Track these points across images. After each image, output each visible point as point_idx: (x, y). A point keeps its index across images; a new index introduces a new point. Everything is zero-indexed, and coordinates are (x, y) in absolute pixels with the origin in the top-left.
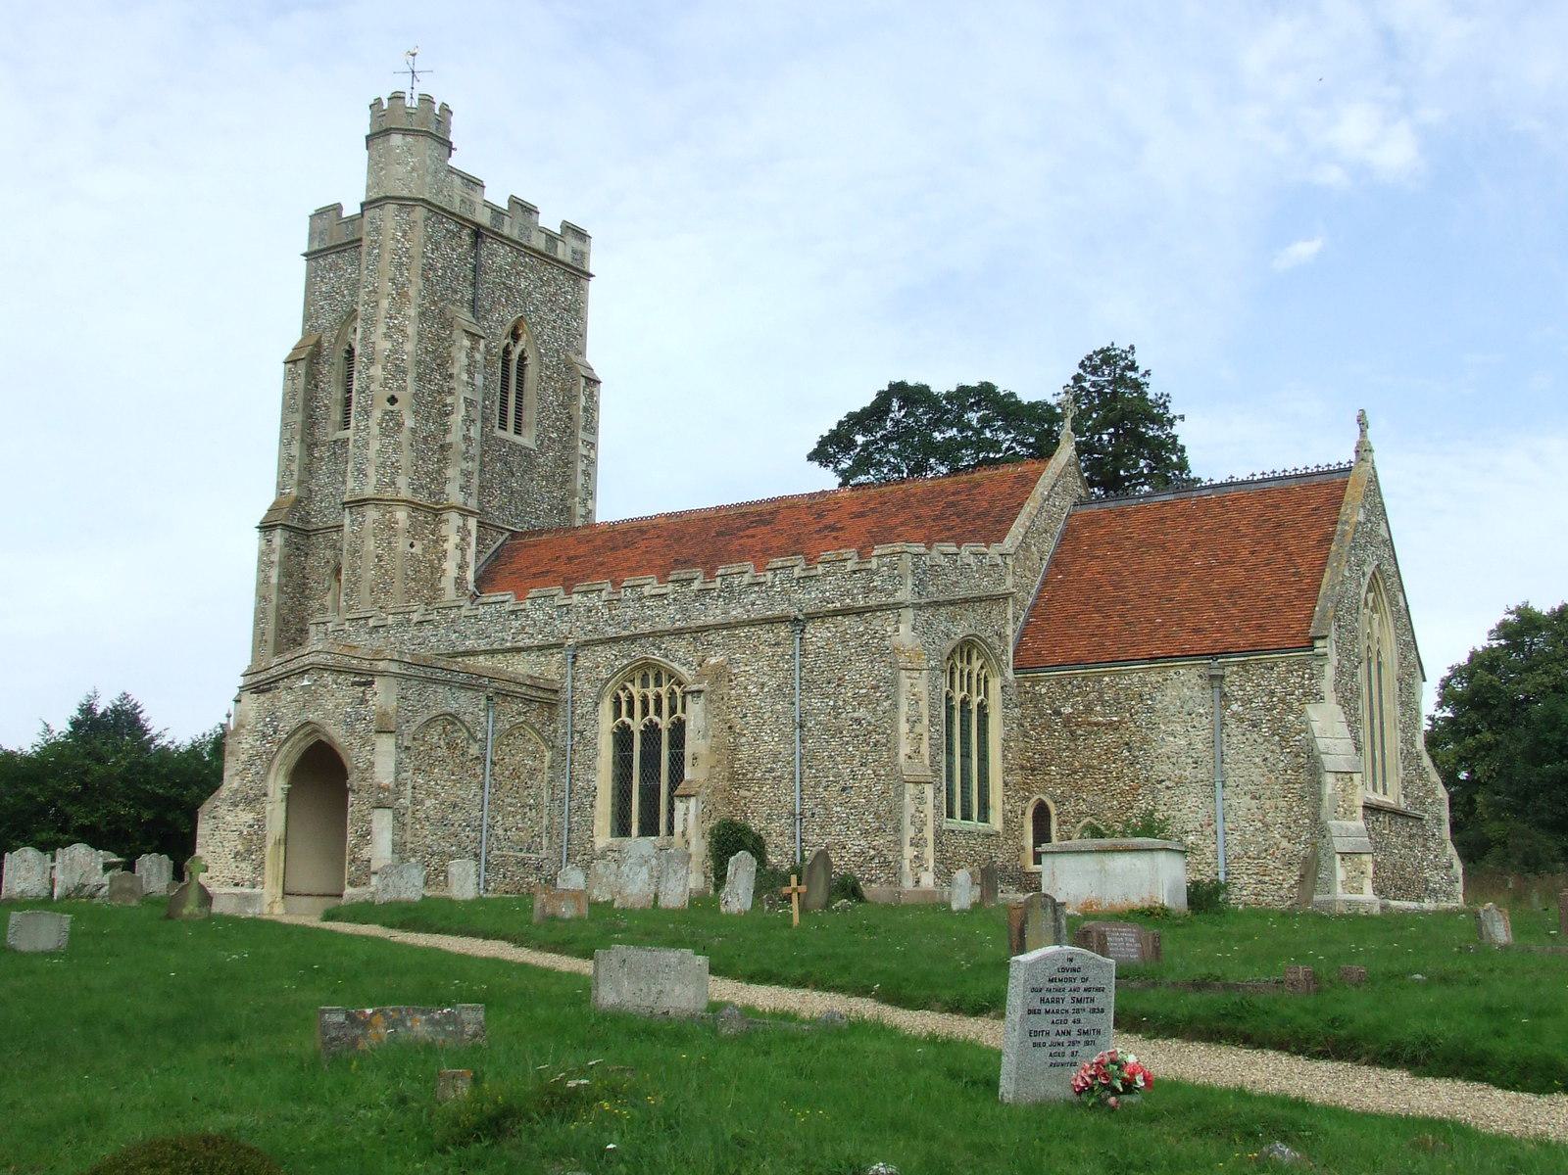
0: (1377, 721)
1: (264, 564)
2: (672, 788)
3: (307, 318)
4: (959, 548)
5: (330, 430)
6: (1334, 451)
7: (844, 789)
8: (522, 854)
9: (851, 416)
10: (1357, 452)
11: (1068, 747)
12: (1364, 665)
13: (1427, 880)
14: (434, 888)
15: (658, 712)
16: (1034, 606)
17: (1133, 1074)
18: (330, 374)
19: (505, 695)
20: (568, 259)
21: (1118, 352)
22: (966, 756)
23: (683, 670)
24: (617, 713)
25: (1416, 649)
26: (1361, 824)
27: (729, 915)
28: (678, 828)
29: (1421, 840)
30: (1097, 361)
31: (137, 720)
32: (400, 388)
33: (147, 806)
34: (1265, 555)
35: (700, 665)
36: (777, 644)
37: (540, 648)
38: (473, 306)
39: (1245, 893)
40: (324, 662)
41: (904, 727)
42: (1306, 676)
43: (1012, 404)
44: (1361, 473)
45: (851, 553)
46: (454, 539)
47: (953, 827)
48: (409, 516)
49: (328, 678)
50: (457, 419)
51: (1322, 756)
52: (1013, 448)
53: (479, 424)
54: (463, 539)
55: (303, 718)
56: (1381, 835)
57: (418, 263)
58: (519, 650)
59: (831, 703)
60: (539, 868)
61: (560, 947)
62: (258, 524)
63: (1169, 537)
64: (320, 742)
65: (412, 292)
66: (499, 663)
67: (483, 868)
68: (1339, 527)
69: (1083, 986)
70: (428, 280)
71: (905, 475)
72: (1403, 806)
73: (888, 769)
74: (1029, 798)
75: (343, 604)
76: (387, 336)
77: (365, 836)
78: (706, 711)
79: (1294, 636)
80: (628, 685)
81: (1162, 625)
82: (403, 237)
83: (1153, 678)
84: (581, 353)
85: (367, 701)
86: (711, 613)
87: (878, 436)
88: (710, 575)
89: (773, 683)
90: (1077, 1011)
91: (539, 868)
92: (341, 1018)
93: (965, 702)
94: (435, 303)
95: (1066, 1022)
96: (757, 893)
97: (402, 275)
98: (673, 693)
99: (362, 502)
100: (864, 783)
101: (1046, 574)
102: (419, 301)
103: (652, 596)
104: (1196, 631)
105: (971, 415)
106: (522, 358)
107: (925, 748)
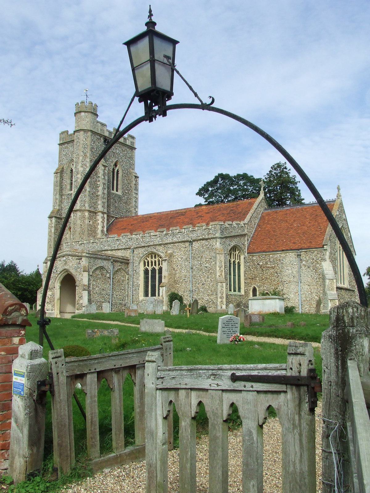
0: (342, 266)
1: (50, 227)
2: (159, 285)
4: (233, 222)
5: (67, 191)
7: (203, 284)
8: (121, 302)
9: (208, 183)
11: (261, 273)
12: (338, 251)
14: (98, 310)
15: (155, 265)
17: (241, 338)
20: (130, 144)
21: (281, 164)
22: (234, 275)
23: (162, 254)
24: (145, 265)
25: (353, 247)
26: (335, 292)
27: (173, 315)
28: (161, 294)
30: (276, 166)
31: (16, 268)
33: (19, 291)
34: (312, 223)
35: (166, 253)
37: (124, 249)
39: (306, 310)
40: (69, 254)
41: (218, 269)
42: (322, 255)
43: (252, 179)
44: (338, 202)
45: (204, 224)
46: (101, 220)
47: (231, 294)
48: (89, 214)
49: (70, 258)
50: (100, 188)
51: (326, 275)
52: (253, 191)
53: (107, 189)
54: (103, 220)
55: (64, 268)
58: (119, 249)
59: (200, 262)
60: (125, 305)
61: (132, 322)
62: (48, 216)
63: (288, 219)
65: (88, 155)
66: (114, 253)
67: (111, 305)
69: (233, 323)
70: (92, 151)
71: (223, 199)
73: (214, 279)
75: (72, 237)
76: (82, 167)
77: (81, 297)
79: (319, 244)
80: (147, 258)
81: (285, 242)
82: (85, 140)
83: (283, 255)
85: (80, 263)
86: (169, 240)
87: (215, 188)
88: (168, 229)
89: (184, 258)
91: (125, 305)
92: (91, 331)
93: (234, 262)
96: (180, 310)
97: (85, 150)
98: (159, 260)
100: (208, 283)
103: (153, 235)
104: (294, 243)
105: (241, 182)
106: (118, 171)
107: (223, 274)
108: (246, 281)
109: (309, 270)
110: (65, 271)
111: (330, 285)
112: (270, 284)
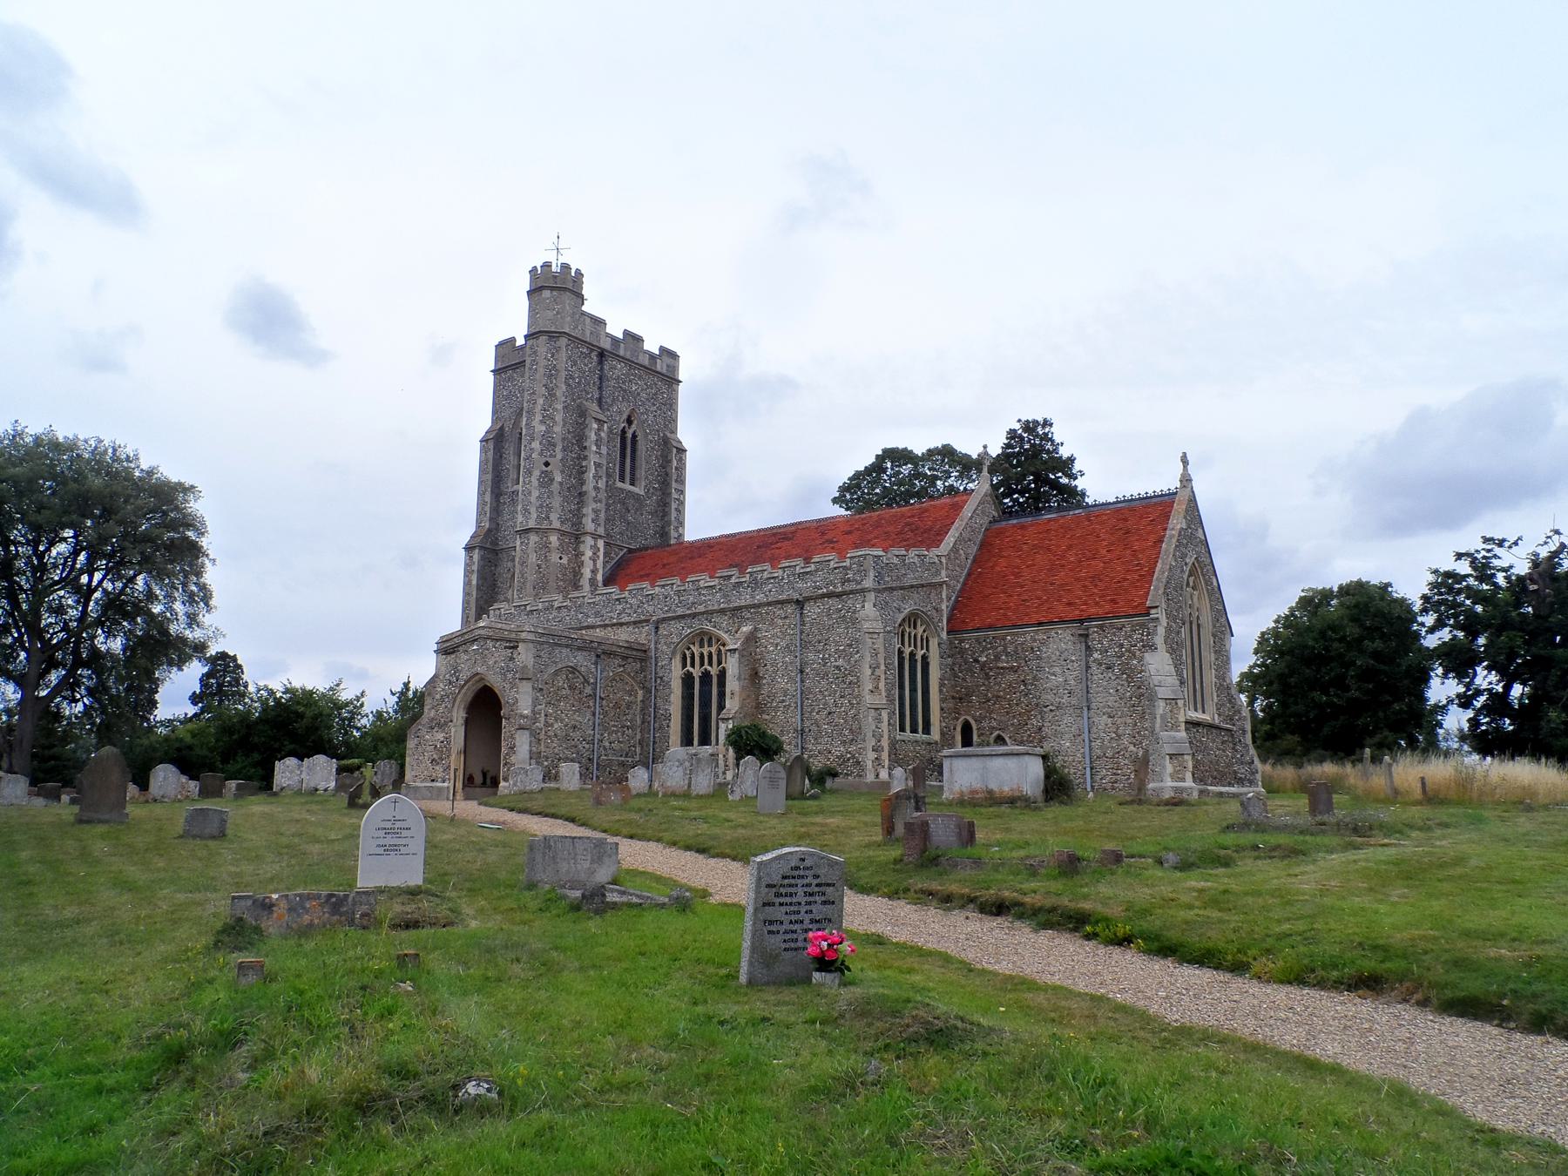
0: (1197, 664)
2: (718, 714)
3: (495, 412)
5: (510, 485)
6: (1164, 481)
7: (830, 713)
10: (1181, 481)
12: (1187, 625)
13: (1235, 772)
15: (710, 664)
16: (960, 591)
18: (509, 450)
19: (609, 654)
22: (913, 690)
24: (684, 666)
26: (1183, 734)
29: (1231, 745)
32: (551, 456)
36: (786, 617)
38: (600, 401)
44: (1183, 496)
46: (589, 553)
48: (558, 539)
49: (490, 644)
53: (604, 479)
54: (594, 554)
56: (1201, 742)
57: (563, 374)
58: (622, 624)
63: (1053, 542)
64: (486, 686)
65: (559, 393)
68: (1168, 532)
69: (815, 882)
72: (1217, 721)
74: (957, 719)
78: (740, 662)
79: (1136, 607)
80: (691, 646)
81: (1046, 601)
83: (1041, 636)
84: (674, 432)
89: (783, 644)
90: (809, 903)
93: (912, 655)
94: (574, 400)
95: (798, 912)
99: (528, 531)
101: (970, 569)
102: (563, 399)
104: (1069, 604)
106: (634, 436)
107: (882, 685)
108: (944, 705)
109: (1110, 675)
110: (477, 678)
111: (1169, 715)
112: (1008, 713)
